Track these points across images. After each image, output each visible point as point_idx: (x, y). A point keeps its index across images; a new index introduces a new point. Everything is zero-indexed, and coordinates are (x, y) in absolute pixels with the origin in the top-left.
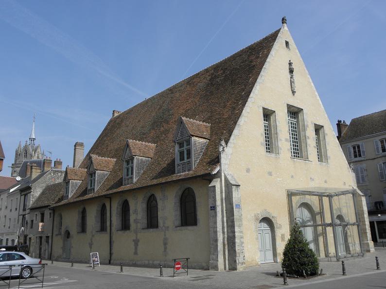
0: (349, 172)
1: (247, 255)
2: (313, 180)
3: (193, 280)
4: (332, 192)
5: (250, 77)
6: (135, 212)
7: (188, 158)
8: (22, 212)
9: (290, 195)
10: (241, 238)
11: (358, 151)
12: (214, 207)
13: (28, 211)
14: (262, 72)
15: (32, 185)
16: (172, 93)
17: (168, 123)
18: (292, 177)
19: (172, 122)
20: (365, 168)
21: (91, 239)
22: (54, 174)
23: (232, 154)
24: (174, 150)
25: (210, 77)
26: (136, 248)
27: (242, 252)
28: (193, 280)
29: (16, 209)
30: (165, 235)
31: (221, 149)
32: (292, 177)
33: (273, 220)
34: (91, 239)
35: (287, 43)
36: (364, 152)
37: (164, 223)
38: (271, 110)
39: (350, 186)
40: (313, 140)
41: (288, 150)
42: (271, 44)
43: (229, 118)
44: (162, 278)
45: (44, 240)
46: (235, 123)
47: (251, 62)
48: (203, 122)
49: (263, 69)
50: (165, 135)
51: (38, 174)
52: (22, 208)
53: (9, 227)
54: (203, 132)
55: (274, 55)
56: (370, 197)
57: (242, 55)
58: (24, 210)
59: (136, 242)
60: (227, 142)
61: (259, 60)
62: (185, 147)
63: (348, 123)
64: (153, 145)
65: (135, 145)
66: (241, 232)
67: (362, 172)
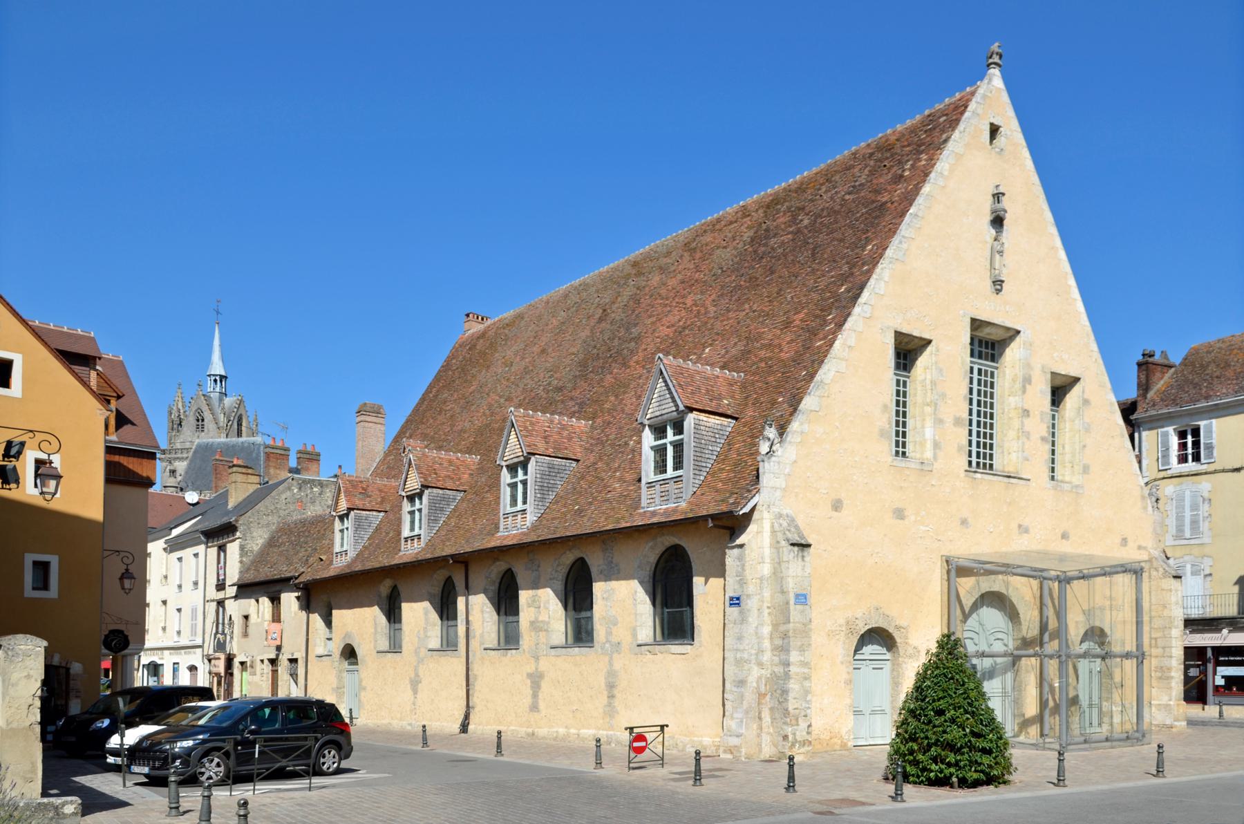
0: (1145, 508)
1: (818, 723)
2: (1027, 531)
3: (674, 780)
4: (1071, 568)
5: (868, 240)
6: (534, 601)
7: (675, 469)
8: (213, 594)
9: (957, 570)
10: (806, 679)
11: (1193, 443)
12: (738, 599)
13: (232, 591)
14: (903, 226)
15: (237, 521)
16: (639, 274)
17: (625, 365)
18: (964, 522)
19: (637, 363)
20: (1206, 495)
21: (416, 669)
22: (300, 488)
23: (795, 461)
24: (639, 442)
25: (751, 233)
26: (535, 696)
27: (806, 716)
28: (674, 780)
29: (196, 583)
30: (611, 664)
31: (764, 448)
32: (964, 522)
33: (896, 635)
34: (416, 669)
35: (994, 131)
36: (1210, 447)
37: (609, 633)
38: (921, 339)
39: (1140, 548)
40: (1042, 420)
41: (960, 449)
42: (944, 136)
43: (797, 360)
44: (600, 772)
45: (283, 666)
46: (812, 376)
47: (877, 192)
48: (722, 368)
49: (907, 218)
50: (616, 396)
51: (252, 488)
52: (212, 581)
53: (179, 633)
54: (720, 398)
55: (946, 173)
56: (1209, 579)
57: (853, 167)
58: (221, 586)
59: (536, 680)
60: (782, 430)
61: (901, 189)
62: (670, 436)
63: (1176, 358)
64: (581, 425)
65: (532, 424)
66: (805, 664)
67: (1195, 507)
